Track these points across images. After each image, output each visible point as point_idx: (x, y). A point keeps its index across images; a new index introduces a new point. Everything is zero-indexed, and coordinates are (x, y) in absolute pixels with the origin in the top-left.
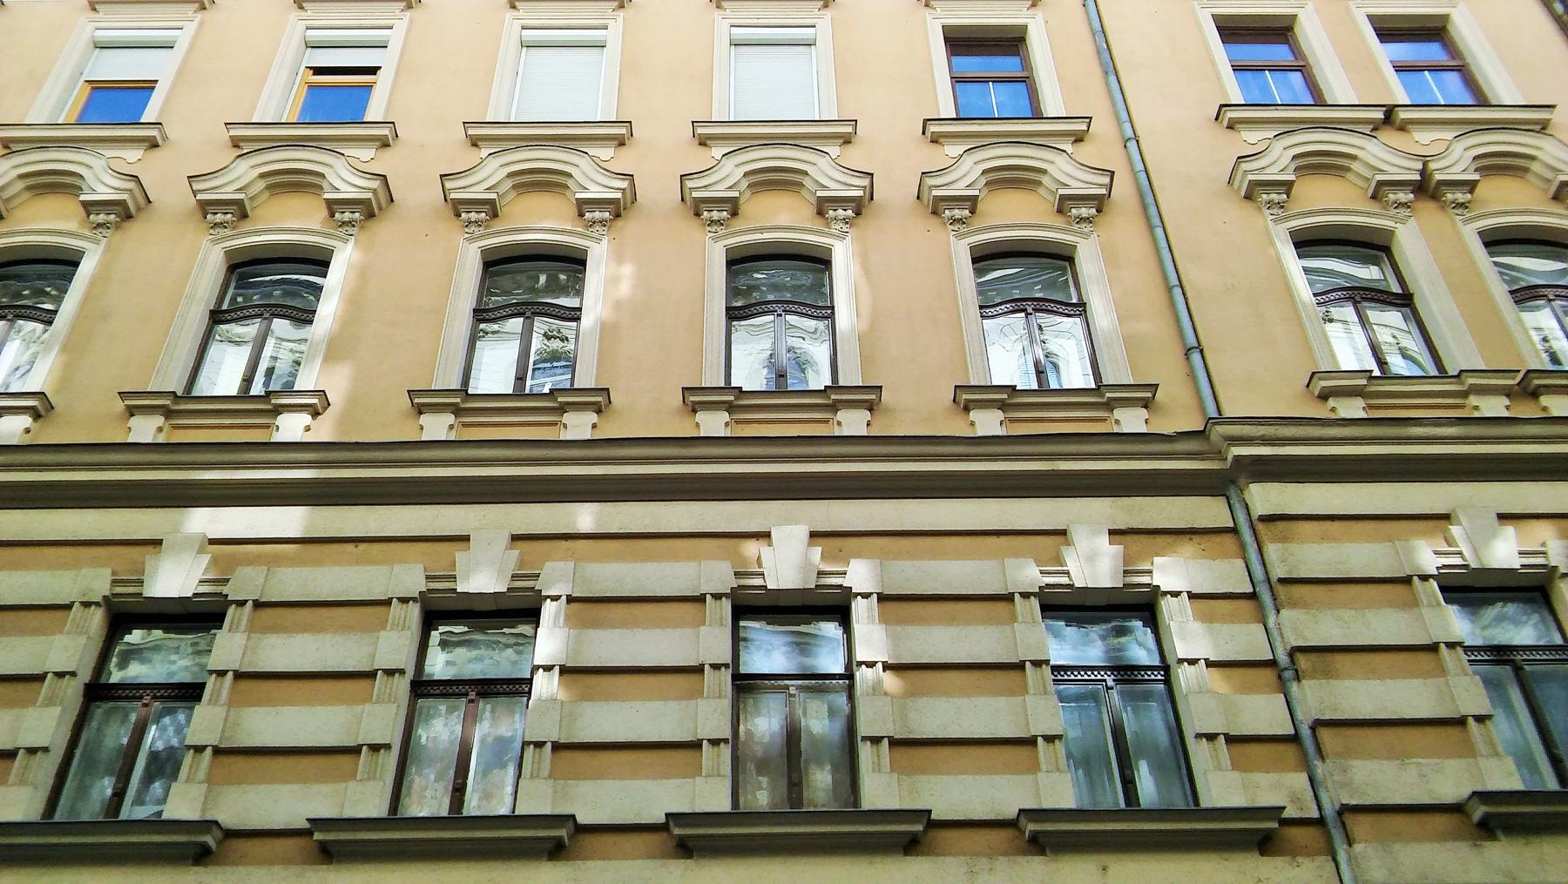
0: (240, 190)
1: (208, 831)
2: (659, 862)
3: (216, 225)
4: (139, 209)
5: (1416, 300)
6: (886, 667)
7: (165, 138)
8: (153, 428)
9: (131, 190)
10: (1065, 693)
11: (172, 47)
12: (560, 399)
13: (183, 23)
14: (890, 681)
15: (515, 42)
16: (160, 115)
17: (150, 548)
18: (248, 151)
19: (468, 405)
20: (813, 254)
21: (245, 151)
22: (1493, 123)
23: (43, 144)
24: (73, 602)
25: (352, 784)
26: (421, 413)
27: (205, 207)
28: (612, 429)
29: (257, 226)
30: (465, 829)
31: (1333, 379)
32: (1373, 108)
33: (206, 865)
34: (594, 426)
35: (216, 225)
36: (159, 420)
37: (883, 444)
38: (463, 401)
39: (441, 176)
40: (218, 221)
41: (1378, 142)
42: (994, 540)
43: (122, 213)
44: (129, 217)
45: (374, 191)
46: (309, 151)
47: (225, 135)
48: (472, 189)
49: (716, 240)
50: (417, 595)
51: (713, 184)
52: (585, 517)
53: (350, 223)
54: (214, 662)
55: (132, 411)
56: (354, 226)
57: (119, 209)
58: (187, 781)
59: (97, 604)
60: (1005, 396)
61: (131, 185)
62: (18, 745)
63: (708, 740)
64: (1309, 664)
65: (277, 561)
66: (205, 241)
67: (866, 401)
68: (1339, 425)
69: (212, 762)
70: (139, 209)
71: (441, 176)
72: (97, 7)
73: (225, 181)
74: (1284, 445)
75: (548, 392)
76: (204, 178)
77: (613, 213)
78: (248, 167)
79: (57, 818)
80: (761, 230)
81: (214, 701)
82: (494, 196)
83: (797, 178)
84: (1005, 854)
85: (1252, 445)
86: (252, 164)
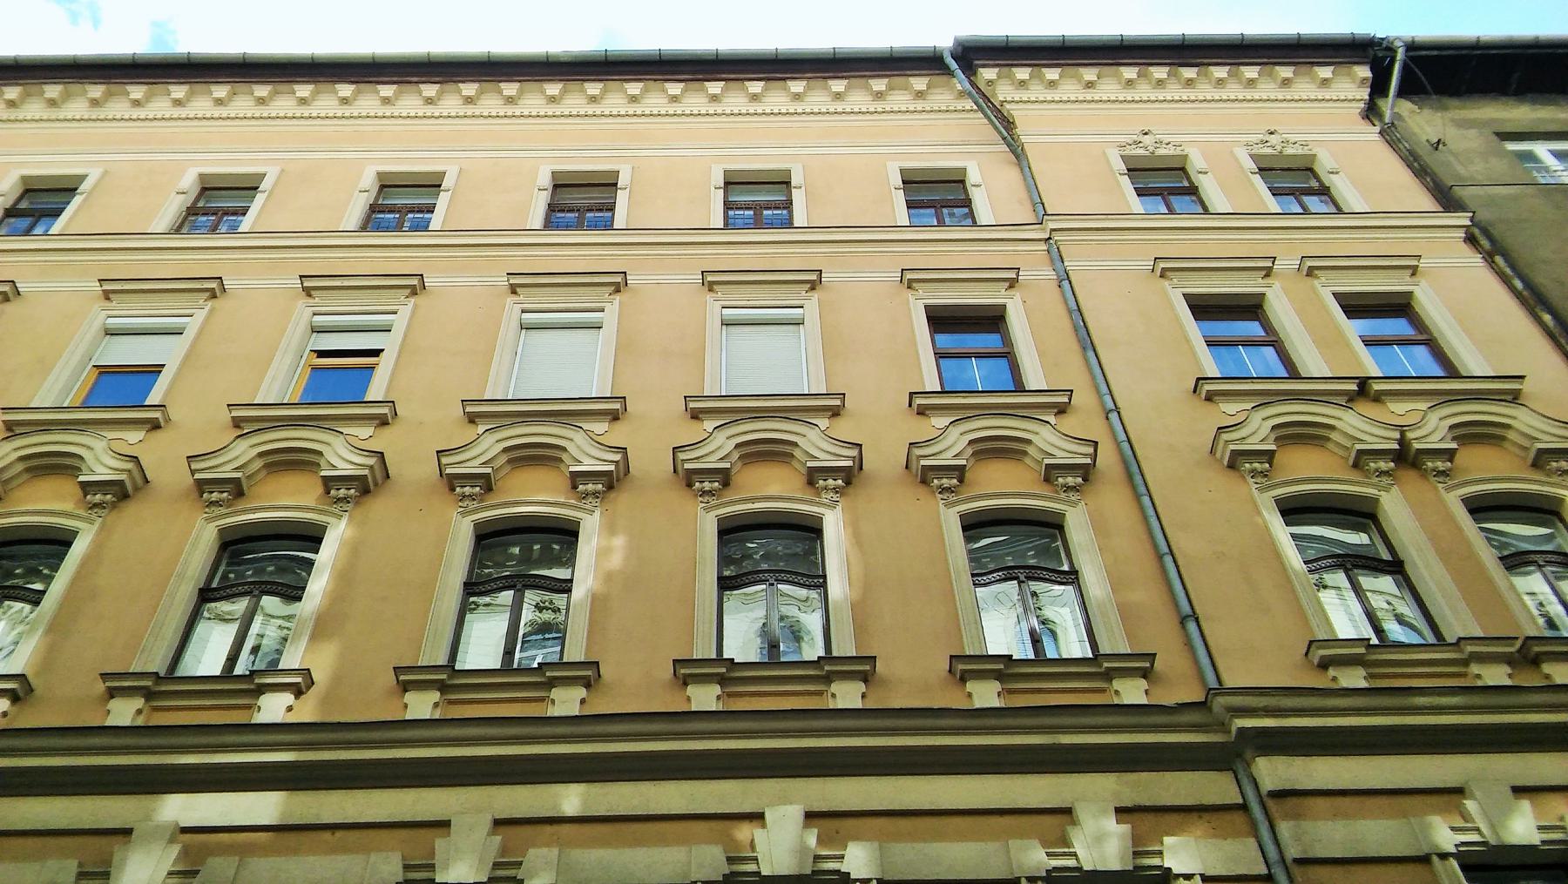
11: (182, 333)
12: (548, 674)
15: (515, 324)
17: (120, 838)
19: (163, 688)
20: (52, 536)
21: (245, 431)
22: (1477, 394)
27: (202, 486)
28: (604, 705)
34: (583, 701)
36: (139, 702)
39: (438, 452)
45: (371, 467)
47: (226, 416)
49: (464, 514)
55: (112, 693)
56: (104, 508)
67: (718, 674)
70: (137, 489)
72: (111, 296)
82: (489, 470)
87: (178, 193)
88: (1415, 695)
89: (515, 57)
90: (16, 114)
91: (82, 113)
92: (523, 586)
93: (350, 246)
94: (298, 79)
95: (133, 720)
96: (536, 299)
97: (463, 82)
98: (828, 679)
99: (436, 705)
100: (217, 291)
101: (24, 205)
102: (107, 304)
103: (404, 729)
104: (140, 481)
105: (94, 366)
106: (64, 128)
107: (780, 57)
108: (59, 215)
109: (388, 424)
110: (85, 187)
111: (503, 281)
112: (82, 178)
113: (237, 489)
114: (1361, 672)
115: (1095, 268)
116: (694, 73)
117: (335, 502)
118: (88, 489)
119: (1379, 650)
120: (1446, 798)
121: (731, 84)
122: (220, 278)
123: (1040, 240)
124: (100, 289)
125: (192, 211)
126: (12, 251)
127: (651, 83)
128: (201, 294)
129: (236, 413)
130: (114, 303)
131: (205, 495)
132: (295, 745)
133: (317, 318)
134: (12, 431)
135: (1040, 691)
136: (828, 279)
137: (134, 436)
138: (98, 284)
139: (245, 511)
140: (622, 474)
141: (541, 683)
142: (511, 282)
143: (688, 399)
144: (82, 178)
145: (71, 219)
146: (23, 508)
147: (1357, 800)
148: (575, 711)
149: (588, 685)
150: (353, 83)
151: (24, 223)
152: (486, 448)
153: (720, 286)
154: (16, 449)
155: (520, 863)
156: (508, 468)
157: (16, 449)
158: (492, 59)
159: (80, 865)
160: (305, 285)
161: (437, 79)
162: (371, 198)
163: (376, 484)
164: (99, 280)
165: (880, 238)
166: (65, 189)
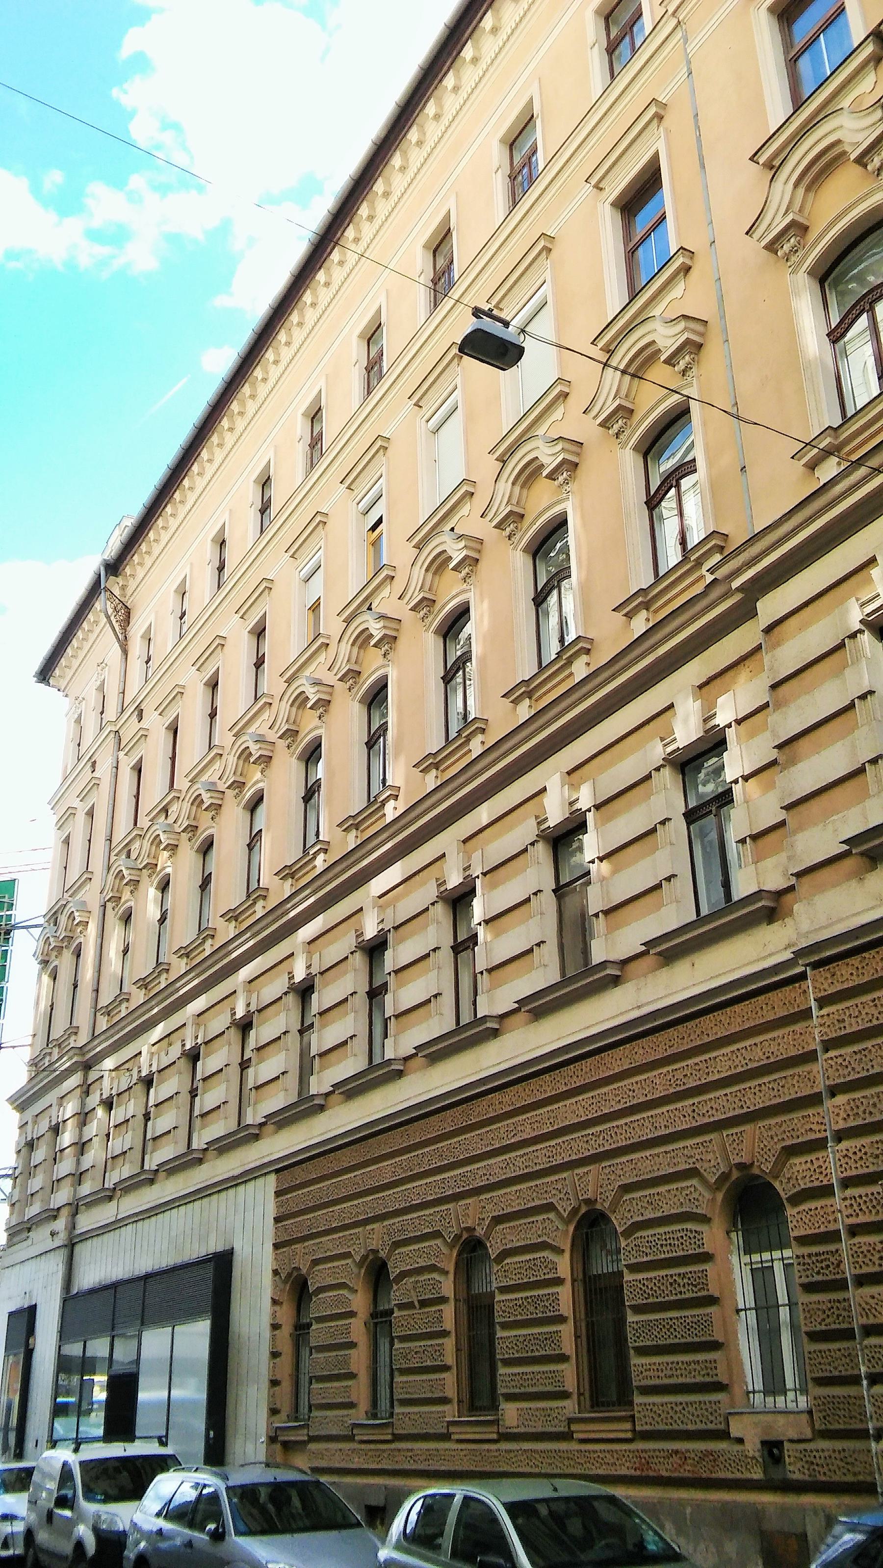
1: (605, 969)
2: (526, 1027)
6: (601, 859)
7: (329, 637)
9: (685, 328)
12: (692, 559)
13: (454, 382)
14: (605, 866)
17: (668, 714)
19: (440, 758)
22: (797, 134)
29: (252, 778)
30: (709, 923)
31: (806, 454)
32: (841, 68)
33: (621, 984)
34: (483, 743)
36: (644, 614)
37: (682, 613)
38: (435, 759)
40: (683, 367)
41: (104, 875)
42: (647, 728)
44: (700, 346)
45: (686, 329)
49: (515, 548)
50: (662, 762)
51: (604, 404)
52: (484, 814)
54: (588, 858)
55: (629, 616)
56: (691, 368)
59: (662, 766)
60: (640, 599)
61: (682, 324)
64: (784, 757)
65: (397, 899)
66: (619, 452)
67: (639, 604)
68: (786, 521)
69: (490, 980)
70: (331, 694)
72: (601, 186)
73: (601, 404)
74: (759, 561)
79: (702, 915)
80: (652, 409)
83: (443, 557)
84: (342, 1103)
85: (741, 574)
88: (833, 486)
90: (484, 63)
93: (525, 215)
95: (435, 783)
96: (210, 668)
97: (358, 209)
98: (570, 662)
101: (614, 32)
103: (694, 605)
106: (506, 54)
107: (334, 212)
108: (641, 14)
109: (690, 268)
111: (588, 188)
114: (834, 460)
115: (723, 16)
116: (450, 54)
119: (846, 426)
121: (475, 36)
123: (675, 29)
125: (611, 49)
126: (487, 263)
127: (436, 92)
128: (650, 127)
133: (302, 573)
135: (670, 601)
139: (367, 679)
141: (565, 664)
146: (373, 669)
149: (588, 652)
150: (320, 268)
151: (625, 47)
153: (504, 302)
154: (506, 482)
156: (525, 491)
157: (506, 482)
159: (537, 817)
161: (347, 222)
163: (702, 335)
165: (661, 41)
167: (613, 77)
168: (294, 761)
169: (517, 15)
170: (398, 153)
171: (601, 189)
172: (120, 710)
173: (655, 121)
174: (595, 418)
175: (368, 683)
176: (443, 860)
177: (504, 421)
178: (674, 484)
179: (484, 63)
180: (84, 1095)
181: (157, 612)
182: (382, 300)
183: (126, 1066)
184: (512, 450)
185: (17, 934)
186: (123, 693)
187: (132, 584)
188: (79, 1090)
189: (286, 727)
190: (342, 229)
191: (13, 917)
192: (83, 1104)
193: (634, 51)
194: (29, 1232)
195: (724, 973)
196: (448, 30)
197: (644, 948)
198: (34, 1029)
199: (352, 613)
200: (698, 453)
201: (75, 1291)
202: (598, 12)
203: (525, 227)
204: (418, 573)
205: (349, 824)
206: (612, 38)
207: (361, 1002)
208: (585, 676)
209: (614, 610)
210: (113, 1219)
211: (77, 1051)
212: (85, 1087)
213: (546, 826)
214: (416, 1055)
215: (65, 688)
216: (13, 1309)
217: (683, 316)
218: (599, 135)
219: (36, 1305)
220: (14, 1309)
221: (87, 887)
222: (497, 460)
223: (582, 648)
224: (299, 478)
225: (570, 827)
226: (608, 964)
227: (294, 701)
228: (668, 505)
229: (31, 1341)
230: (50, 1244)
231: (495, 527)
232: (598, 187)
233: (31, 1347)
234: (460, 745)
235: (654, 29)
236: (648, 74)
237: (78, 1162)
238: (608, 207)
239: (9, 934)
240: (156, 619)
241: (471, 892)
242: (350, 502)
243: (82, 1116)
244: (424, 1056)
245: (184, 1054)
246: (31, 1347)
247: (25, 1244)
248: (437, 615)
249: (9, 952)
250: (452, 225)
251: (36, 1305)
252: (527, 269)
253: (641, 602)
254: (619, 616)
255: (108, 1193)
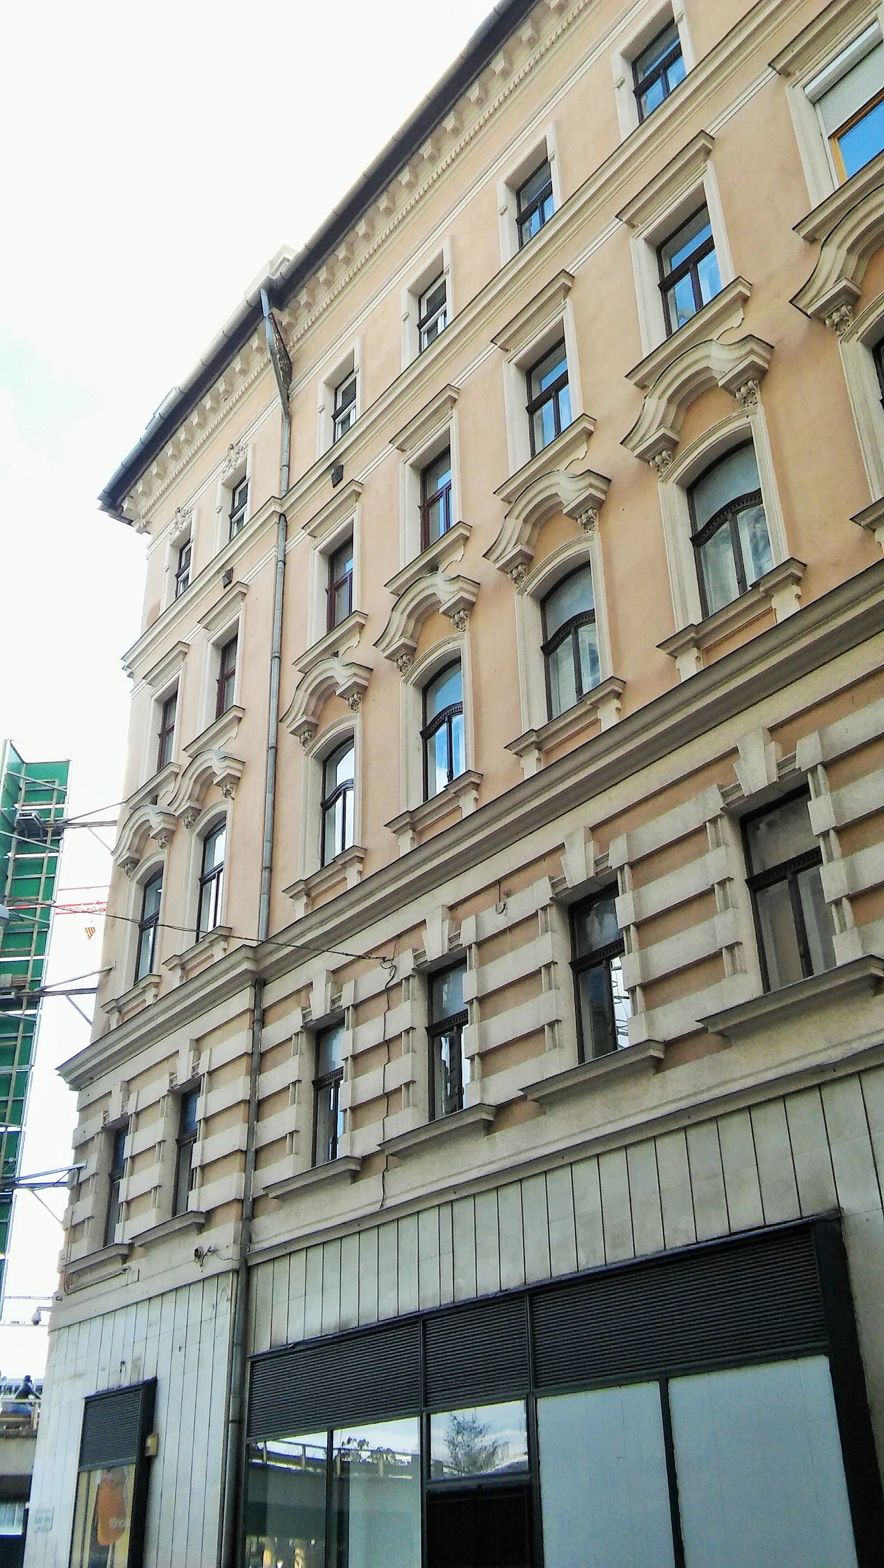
0: (839, 278)
3: (837, 326)
4: (768, 362)
5: (320, 801)
8: (472, 802)
10: (723, 906)
11: (882, 41)
15: (806, 106)
16: (736, 268)
18: (825, 238)
20: (734, 443)
21: (823, 240)
23: (849, 209)
24: (537, 911)
25: (724, 982)
26: (874, 531)
27: (818, 317)
28: (490, 794)
35: (837, 326)
39: (791, 302)
43: (465, 608)
46: (691, 353)
47: (798, 239)
48: (826, 289)
50: (720, 812)
51: (824, 284)
53: (843, 321)
54: (817, 829)
55: (674, 655)
57: (750, 373)
58: (842, 931)
59: (720, 816)
61: (354, 670)
62: (719, 947)
63: (726, 947)
71: (791, 302)
75: (751, 588)
76: (629, 438)
77: (525, 561)
78: (400, 614)
81: (831, 859)
82: (844, 283)
86: (837, 244)
87: (502, 214)
89: (242, 314)
90: (375, 242)
91: (528, 63)
92: (733, 514)
94: (176, 427)
99: (539, 760)
100: (707, 144)
102: (509, 355)
104: (364, 674)
105: (829, 138)
108: (551, 193)
110: (447, 262)
112: (441, 257)
113: (670, 445)
117: (744, 402)
118: (822, 315)
120: (847, 697)
122: (702, 131)
124: (496, 346)
129: (805, 231)
130: (798, 73)
131: (827, 322)
132: (117, 1053)
134: (511, 502)
136: (459, 384)
137: (735, 320)
138: (618, 220)
139: (329, 730)
140: (475, 590)
142: (499, 344)
143: (740, 279)
144: (441, 257)
145: (563, 181)
147: (676, 789)
148: (795, 607)
152: (655, 406)
154: (402, 613)
155: (794, 757)
157: (402, 613)
158: (127, 466)
160: (778, 69)
162: (630, 85)
164: (492, 341)
166: (436, 273)
167: (522, 245)
168: (411, 688)
169: (482, 117)
170: (501, 55)
171: (633, 226)
172: (284, 487)
173: (702, 154)
174: (384, 650)
175: (322, 742)
176: (423, 928)
177: (401, 557)
178: (446, 720)
179: (517, 76)
180: (257, 1027)
181: (364, 338)
182: (445, 246)
183: (382, 953)
184: (527, 486)
185: (68, 833)
186: (288, 466)
187: (305, 320)
188: (247, 1018)
189: (304, 719)
190: (128, 489)
191: (65, 811)
192: (256, 1040)
193: (667, 92)
194: (124, 1262)
195: (454, 1175)
196: (162, 421)
197: (700, 1025)
198: (106, 961)
199: (535, 473)
200: (600, 604)
201: (263, 1345)
202: (625, 55)
203: (771, 28)
204: (400, 619)
205: (299, 889)
206: (522, 211)
207: (306, 1090)
208: (696, 673)
209: (385, 826)
210: (376, 1208)
211: (250, 954)
212: (257, 1013)
213: (422, 960)
214: (522, 1099)
215: (146, 513)
216: (92, 1392)
217: (750, 335)
218: (477, 327)
219: (154, 1382)
220: (93, 1393)
221: (233, 733)
222: (502, 500)
223: (613, 691)
224: (408, 355)
225: (594, 891)
226: (652, 1044)
227: (532, 512)
228: (565, 653)
229: (150, 1442)
230: (195, 1272)
231: (387, 658)
232: (631, 224)
233: (151, 1452)
234: (752, 605)
235: (562, 207)
236: (503, 300)
237: (251, 1133)
238: (316, 552)
239: (59, 834)
240: (363, 346)
241: (610, 890)
242: (401, 465)
243: (256, 1057)
244: (535, 1100)
245: (419, 971)
246: (151, 1452)
247: (123, 1280)
248: (534, 577)
249: (59, 859)
250: (676, 14)
251: (154, 1382)
252: (662, 188)
253: (692, 639)
254: (662, 654)
255: (353, 1167)
